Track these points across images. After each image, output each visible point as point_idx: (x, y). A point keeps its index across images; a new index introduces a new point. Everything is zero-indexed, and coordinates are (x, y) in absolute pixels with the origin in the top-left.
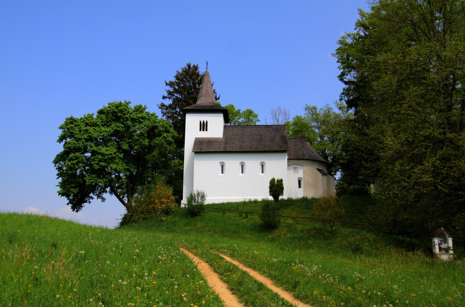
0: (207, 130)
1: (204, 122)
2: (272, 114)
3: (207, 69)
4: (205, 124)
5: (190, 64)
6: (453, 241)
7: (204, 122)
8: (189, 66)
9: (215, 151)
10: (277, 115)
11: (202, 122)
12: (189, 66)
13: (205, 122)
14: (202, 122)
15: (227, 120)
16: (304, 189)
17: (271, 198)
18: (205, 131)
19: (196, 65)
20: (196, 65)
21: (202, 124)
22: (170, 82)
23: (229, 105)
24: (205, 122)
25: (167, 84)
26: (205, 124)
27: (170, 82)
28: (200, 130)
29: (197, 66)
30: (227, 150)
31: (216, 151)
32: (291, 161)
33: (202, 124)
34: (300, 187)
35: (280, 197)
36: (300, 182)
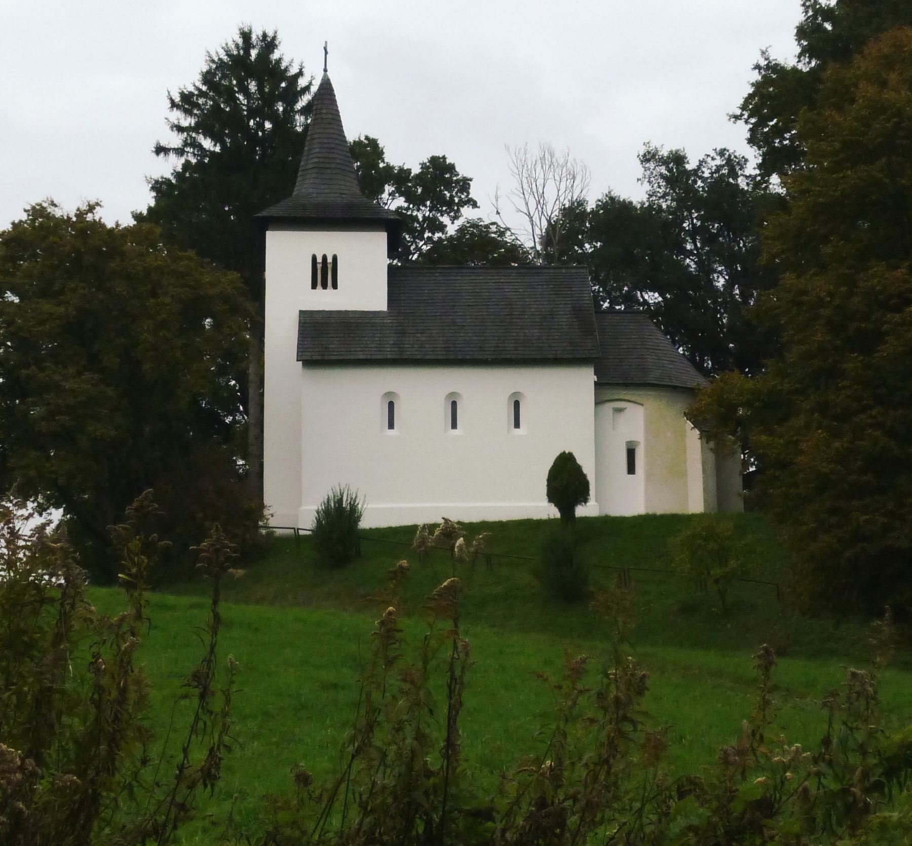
0: (335, 286)
1: (325, 258)
2: (520, 174)
3: (325, 70)
4: (330, 266)
5: (250, 31)
6: (120, 573)
7: (325, 258)
8: (246, 36)
9: (369, 357)
10: (540, 182)
11: (319, 260)
12: (246, 36)
13: (330, 260)
14: (319, 260)
15: (395, 248)
16: (649, 476)
17: (553, 512)
18: (330, 290)
19: (270, 34)
20: (270, 34)
21: (319, 266)
22: (183, 95)
23: (363, 139)
24: (330, 260)
25: (174, 105)
26: (330, 266)
27: (183, 95)
28: (314, 286)
29: (274, 38)
30: (407, 355)
31: (374, 357)
32: (610, 393)
33: (319, 266)
34: (631, 469)
35: (581, 511)
36: (631, 454)
